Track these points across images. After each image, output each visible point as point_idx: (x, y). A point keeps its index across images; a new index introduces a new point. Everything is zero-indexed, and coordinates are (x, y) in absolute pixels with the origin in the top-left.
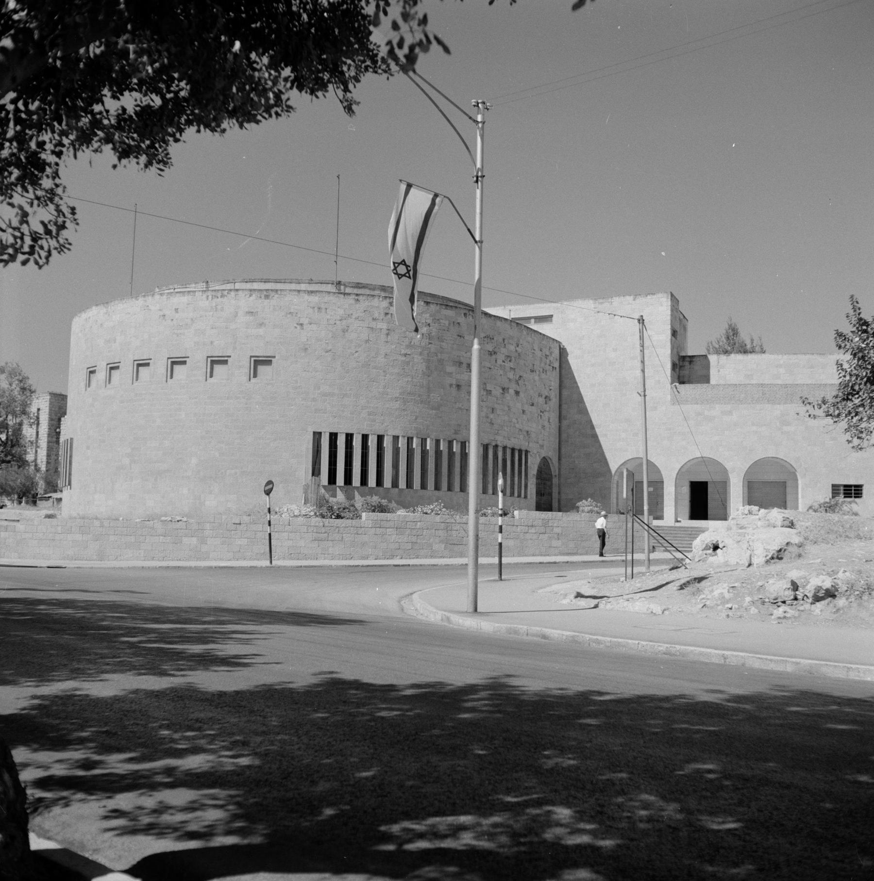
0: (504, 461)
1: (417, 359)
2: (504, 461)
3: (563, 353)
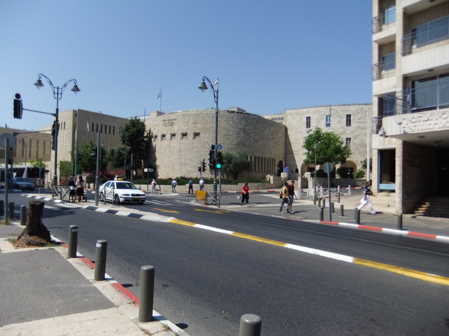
0: (265, 163)
1: (242, 132)
2: (265, 163)
3: (286, 129)
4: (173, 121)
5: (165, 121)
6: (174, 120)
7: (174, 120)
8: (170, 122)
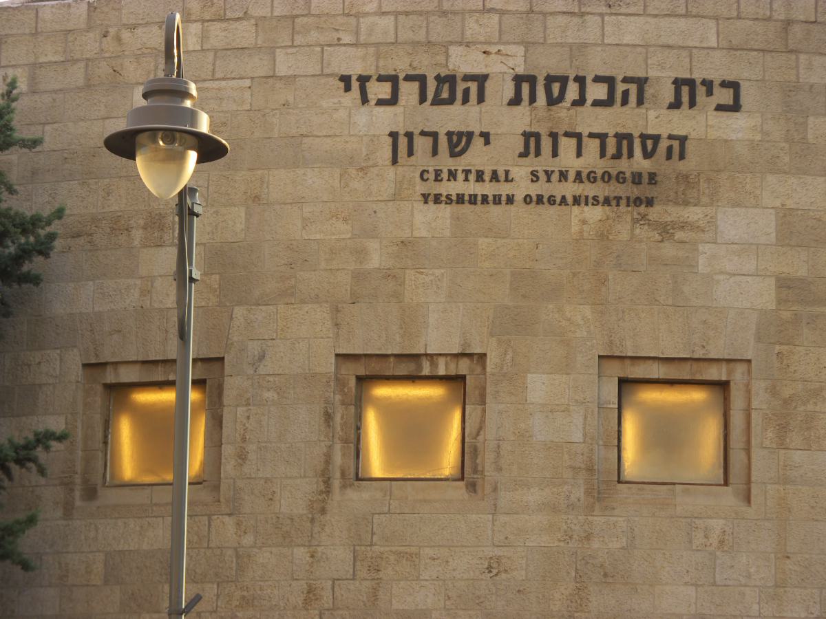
4: (658, 120)
5: (447, 89)
6: (686, 91)
7: (686, 91)
8: (592, 120)
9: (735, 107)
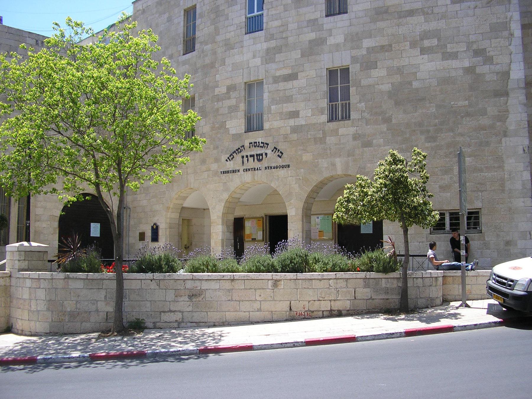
9: (280, 157)
